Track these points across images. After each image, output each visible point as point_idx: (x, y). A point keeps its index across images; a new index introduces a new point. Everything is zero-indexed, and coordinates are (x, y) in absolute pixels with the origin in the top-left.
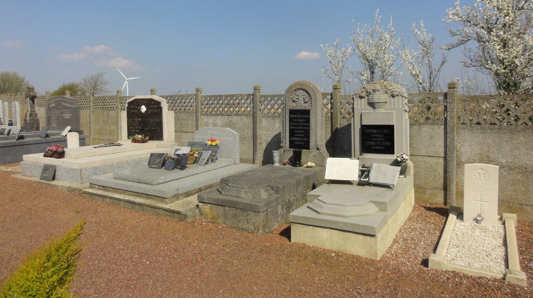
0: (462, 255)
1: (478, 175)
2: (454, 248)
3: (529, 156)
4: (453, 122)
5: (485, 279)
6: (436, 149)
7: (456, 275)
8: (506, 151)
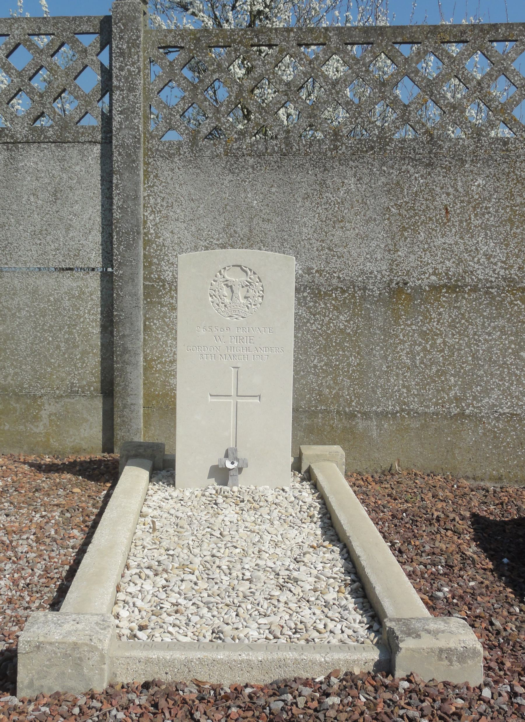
0: (181, 601)
1: (226, 291)
2: (148, 577)
3: (374, 244)
4: (131, 128)
5: (307, 691)
6: (72, 239)
7: (162, 703)
8: (305, 230)
